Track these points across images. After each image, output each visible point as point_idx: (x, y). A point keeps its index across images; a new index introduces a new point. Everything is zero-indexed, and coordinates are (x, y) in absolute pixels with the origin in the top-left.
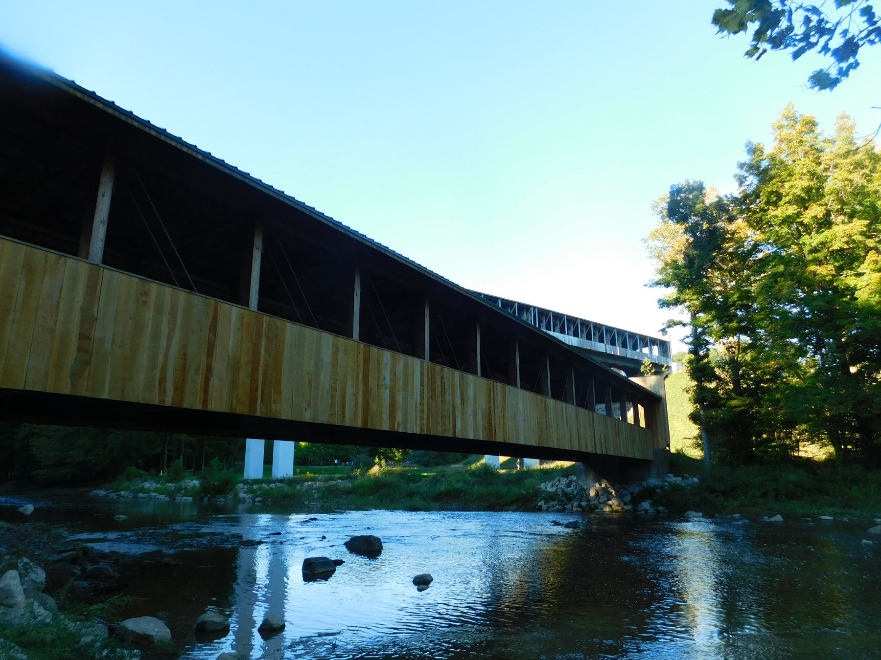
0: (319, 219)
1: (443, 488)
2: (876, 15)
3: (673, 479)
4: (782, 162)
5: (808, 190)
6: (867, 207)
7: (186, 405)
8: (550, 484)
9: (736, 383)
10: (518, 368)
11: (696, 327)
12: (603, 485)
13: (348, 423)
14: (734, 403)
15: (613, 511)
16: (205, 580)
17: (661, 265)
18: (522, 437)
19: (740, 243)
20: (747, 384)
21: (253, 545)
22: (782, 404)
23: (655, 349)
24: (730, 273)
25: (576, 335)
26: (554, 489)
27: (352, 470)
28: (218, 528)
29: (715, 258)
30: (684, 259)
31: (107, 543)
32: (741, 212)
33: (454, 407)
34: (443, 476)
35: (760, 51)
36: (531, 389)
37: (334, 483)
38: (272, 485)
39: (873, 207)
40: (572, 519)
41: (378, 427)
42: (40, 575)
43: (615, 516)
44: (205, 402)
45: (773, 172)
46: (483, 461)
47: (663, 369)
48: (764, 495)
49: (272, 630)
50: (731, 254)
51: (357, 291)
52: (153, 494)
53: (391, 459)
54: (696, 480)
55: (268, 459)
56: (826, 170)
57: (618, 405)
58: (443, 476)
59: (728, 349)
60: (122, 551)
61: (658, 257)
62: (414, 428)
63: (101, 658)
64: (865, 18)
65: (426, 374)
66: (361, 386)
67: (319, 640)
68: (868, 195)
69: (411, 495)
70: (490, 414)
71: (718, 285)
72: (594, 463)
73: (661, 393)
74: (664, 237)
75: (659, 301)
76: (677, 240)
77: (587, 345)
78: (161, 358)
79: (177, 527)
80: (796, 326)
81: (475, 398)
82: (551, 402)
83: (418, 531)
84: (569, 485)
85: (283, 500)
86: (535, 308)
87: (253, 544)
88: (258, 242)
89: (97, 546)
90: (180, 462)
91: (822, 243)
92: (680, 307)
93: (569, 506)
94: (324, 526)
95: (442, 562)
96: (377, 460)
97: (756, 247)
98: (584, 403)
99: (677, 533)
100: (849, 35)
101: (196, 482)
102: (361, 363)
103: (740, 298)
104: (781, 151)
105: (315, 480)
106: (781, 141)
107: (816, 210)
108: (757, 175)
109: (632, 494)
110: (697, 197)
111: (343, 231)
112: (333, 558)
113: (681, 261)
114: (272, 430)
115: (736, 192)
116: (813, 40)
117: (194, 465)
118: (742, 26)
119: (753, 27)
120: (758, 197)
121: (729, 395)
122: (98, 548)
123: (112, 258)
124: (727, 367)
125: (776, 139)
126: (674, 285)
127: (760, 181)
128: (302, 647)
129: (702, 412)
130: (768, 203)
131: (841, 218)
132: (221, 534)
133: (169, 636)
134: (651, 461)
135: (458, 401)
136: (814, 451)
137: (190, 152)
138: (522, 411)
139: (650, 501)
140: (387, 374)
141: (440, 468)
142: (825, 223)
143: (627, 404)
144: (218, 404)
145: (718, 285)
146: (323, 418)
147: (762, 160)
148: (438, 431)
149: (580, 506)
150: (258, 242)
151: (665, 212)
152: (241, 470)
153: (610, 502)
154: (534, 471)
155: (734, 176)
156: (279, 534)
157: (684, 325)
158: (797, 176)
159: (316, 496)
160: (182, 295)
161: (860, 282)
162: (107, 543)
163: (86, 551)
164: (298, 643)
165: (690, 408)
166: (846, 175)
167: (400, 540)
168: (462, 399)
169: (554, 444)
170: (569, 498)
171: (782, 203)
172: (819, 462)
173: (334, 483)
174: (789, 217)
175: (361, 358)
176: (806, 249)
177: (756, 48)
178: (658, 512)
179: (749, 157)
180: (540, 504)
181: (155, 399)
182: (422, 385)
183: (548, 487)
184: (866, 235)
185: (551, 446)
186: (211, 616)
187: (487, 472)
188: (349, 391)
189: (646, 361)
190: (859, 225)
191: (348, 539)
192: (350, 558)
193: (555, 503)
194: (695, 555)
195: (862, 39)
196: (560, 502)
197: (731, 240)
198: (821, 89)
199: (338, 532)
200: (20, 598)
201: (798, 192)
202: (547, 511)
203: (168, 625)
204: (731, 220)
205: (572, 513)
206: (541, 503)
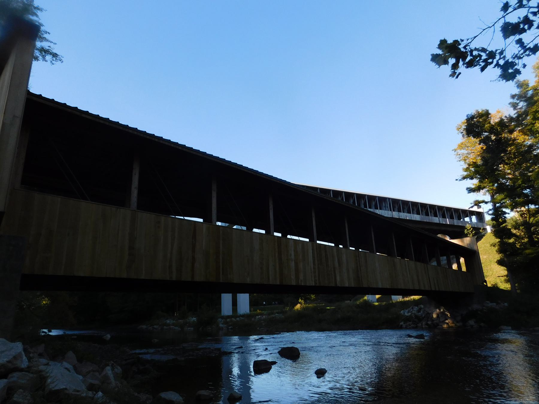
2: (525, 43)
8: (407, 311)
9: (530, 238)
10: (374, 241)
12: (442, 310)
14: (527, 251)
15: (449, 327)
17: (466, 166)
19: (519, 146)
21: (226, 354)
24: (515, 166)
25: (418, 213)
26: (410, 314)
30: (481, 160)
31: (149, 355)
32: (517, 126)
35: (457, 74)
37: (273, 316)
38: (238, 319)
40: (419, 333)
42: (119, 370)
46: (366, 298)
47: (481, 231)
50: (514, 153)
54: (506, 304)
57: (445, 257)
59: (521, 215)
61: (465, 160)
62: (311, 282)
64: (518, 45)
71: (509, 174)
72: (434, 297)
73: (475, 248)
74: (468, 147)
75: (467, 189)
76: (475, 148)
77: (426, 219)
84: (419, 311)
85: (246, 327)
86: (389, 199)
93: (420, 325)
94: (268, 342)
96: (300, 300)
98: (420, 258)
99: (497, 341)
100: (506, 59)
101: (194, 319)
103: (523, 182)
108: (525, 101)
110: (485, 121)
112: (270, 360)
113: (479, 162)
114: (235, 289)
115: (513, 113)
119: (452, 61)
120: (527, 115)
121: (524, 246)
123: (142, 206)
124: (521, 228)
125: (536, 76)
126: (476, 177)
127: (527, 105)
129: (506, 259)
132: (209, 348)
143: (451, 257)
144: (199, 278)
145: (509, 174)
146: (257, 281)
147: (528, 91)
149: (427, 324)
151: (464, 132)
152: (219, 310)
153: (447, 321)
156: (241, 347)
157: (486, 203)
162: (149, 355)
169: (402, 286)
173: (273, 316)
179: (519, 90)
180: (401, 324)
182: (313, 257)
183: (406, 313)
185: (400, 287)
191: (280, 349)
193: (411, 323)
196: (414, 322)
198: (506, 81)
199: (275, 345)
200: (112, 380)
202: (406, 328)
204: (511, 132)
205: (422, 329)
206: (402, 323)
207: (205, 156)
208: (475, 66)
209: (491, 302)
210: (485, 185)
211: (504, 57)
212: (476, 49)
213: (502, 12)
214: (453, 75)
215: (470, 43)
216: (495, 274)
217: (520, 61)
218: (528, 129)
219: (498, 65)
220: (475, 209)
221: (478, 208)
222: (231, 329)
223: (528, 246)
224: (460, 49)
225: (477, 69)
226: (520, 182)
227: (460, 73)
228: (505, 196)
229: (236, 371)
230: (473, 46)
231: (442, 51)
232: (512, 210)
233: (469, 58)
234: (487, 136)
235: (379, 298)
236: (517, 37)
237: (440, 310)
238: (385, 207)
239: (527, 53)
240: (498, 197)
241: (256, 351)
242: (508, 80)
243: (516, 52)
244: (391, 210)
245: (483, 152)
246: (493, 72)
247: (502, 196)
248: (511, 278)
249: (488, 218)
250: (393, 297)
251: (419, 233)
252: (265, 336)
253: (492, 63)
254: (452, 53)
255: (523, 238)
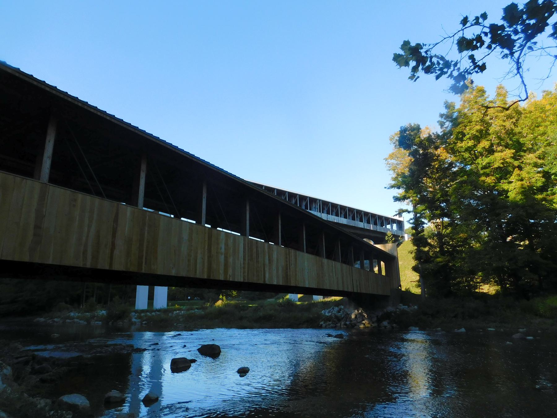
0: (181, 153)
1: (261, 314)
3: (402, 307)
4: (465, 114)
5: (480, 131)
6: (515, 141)
7: (99, 267)
8: (328, 311)
10: (305, 240)
11: (416, 213)
12: (360, 311)
13: (198, 275)
14: (439, 260)
15: (365, 327)
16: (112, 371)
17: (394, 175)
18: (307, 282)
19: (442, 162)
20: (447, 248)
22: (466, 260)
23: (395, 226)
24: (436, 180)
25: (345, 217)
26: (330, 314)
27: (204, 303)
28: (118, 341)
29: (427, 171)
30: (409, 171)
31: (47, 352)
32: (442, 144)
33: (264, 265)
34: (262, 307)
35: (416, 77)
36: (312, 253)
37: (193, 311)
38: (153, 313)
39: (518, 142)
40: (339, 332)
41: (217, 278)
43: (367, 330)
44: (111, 264)
45: (460, 120)
48: (455, 316)
49: (150, 401)
50: (437, 169)
51: (205, 195)
52: (76, 320)
53: (230, 296)
54: (416, 307)
55: (151, 297)
56: (491, 119)
58: (262, 307)
59: (436, 226)
60: (57, 357)
61: (394, 170)
63: (50, 416)
64: (470, 61)
65: (247, 246)
66: (206, 253)
67: (178, 406)
68: (514, 134)
69: (241, 318)
70: (287, 269)
71: (430, 187)
72: (355, 298)
73: (395, 254)
74: (398, 158)
76: (405, 159)
78: (84, 238)
79: (92, 341)
80: (473, 213)
81: (277, 260)
82: (325, 261)
83: (242, 341)
84: (339, 312)
85: (161, 323)
86: (320, 200)
87: (142, 351)
88: (144, 167)
89: (41, 354)
90: (93, 299)
91: (489, 163)
92: (406, 201)
93: (339, 325)
95: (263, 359)
96: (221, 297)
97: (451, 165)
98: (346, 261)
99: (404, 340)
101: (104, 312)
102: (207, 239)
103: (442, 196)
104: (464, 107)
105: (181, 310)
106: (465, 101)
107: (484, 144)
108: (451, 121)
109: (377, 316)
110: (416, 134)
111: (195, 160)
112: (189, 358)
113: (407, 173)
114: (153, 280)
115: (440, 131)
116: (445, 70)
117: (102, 301)
118: (407, 64)
119: (413, 63)
120: (451, 135)
121: (436, 255)
122: (41, 355)
123: (53, 180)
125: (461, 100)
126: (403, 187)
127: (452, 125)
128: (168, 409)
129: (420, 266)
130: (457, 139)
131: (499, 148)
132: (120, 345)
133: (88, 405)
134: (389, 296)
135: (267, 262)
136: (488, 289)
137: (102, 115)
138: (307, 267)
139: (388, 321)
140: (223, 246)
141: (260, 302)
142: (490, 151)
143: (374, 260)
144: (118, 266)
145: (430, 187)
146: (183, 274)
148: (254, 280)
149: (345, 324)
150: (144, 167)
151: (397, 143)
152: (134, 304)
153: (364, 322)
154: (319, 302)
155: (438, 122)
156: (157, 344)
157: (409, 212)
158: (474, 123)
159: (181, 320)
160: (97, 200)
161: (511, 187)
162: (47, 352)
163: (34, 357)
164: (166, 408)
165: (413, 263)
166: (501, 123)
167: (232, 347)
168: (269, 260)
169: (327, 287)
170: (339, 319)
171: (465, 139)
172: (490, 295)
173: (193, 311)
174: (469, 147)
175: (207, 235)
176: (480, 166)
177: (414, 76)
178: (393, 327)
179: (446, 110)
180: (321, 323)
181: (80, 264)
182: (244, 252)
184: (515, 158)
185: (325, 288)
186: (114, 393)
187: (290, 303)
188: (199, 256)
189: (389, 233)
190: (509, 153)
192: (201, 359)
193: (330, 323)
194: (416, 354)
195: (472, 70)
196: (334, 322)
197: (437, 160)
201: (474, 132)
202: (326, 328)
203: (88, 399)
204: (436, 148)
205: (340, 329)
207: (137, 132)
208: (432, 73)
209: (404, 305)
210: (410, 195)
211: (459, 69)
212: (435, 56)
213: (461, 25)
214: (412, 77)
215: (432, 48)
216: (409, 280)
217: (470, 76)
218: (451, 148)
219: (451, 76)
220: (397, 218)
221: (399, 217)
222: (145, 324)
223: (439, 255)
224: (421, 53)
225: (433, 75)
226: (439, 196)
227: (418, 77)
228: (426, 207)
229: (147, 369)
230: (433, 52)
231: (404, 52)
232: (429, 221)
233: (428, 63)
234: (416, 149)
235: (301, 298)
236: (470, 53)
237: (358, 311)
238: (315, 208)
239: (476, 69)
240: (420, 207)
241: (173, 348)
242: (456, 93)
243: (468, 67)
244: (320, 212)
245: (411, 164)
246: (446, 82)
247: (424, 207)
248: (423, 282)
249: (407, 226)
250: (315, 297)
251: (341, 237)
252: (184, 333)
253: (446, 73)
254: (414, 56)
255: (435, 248)
